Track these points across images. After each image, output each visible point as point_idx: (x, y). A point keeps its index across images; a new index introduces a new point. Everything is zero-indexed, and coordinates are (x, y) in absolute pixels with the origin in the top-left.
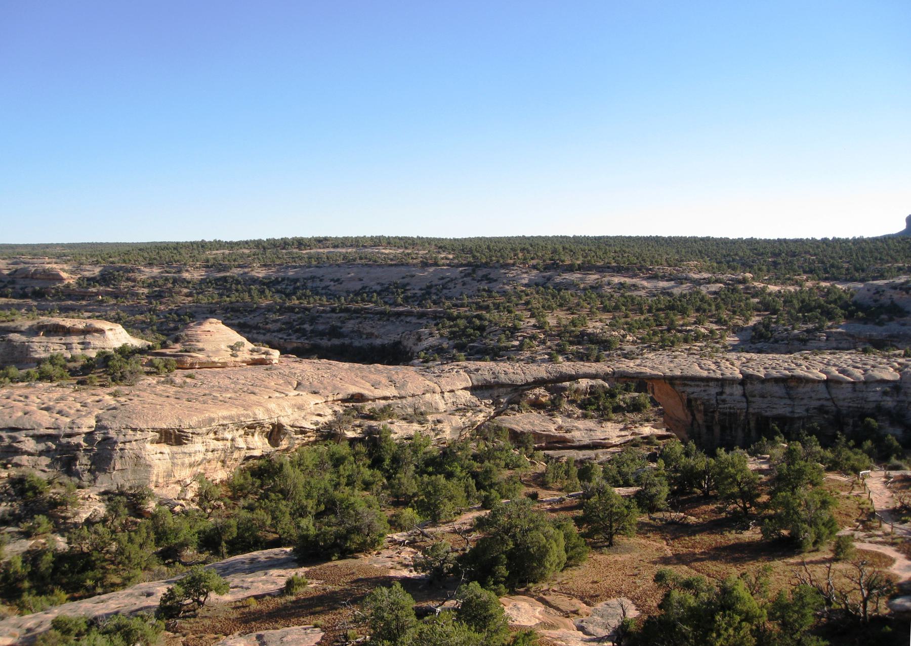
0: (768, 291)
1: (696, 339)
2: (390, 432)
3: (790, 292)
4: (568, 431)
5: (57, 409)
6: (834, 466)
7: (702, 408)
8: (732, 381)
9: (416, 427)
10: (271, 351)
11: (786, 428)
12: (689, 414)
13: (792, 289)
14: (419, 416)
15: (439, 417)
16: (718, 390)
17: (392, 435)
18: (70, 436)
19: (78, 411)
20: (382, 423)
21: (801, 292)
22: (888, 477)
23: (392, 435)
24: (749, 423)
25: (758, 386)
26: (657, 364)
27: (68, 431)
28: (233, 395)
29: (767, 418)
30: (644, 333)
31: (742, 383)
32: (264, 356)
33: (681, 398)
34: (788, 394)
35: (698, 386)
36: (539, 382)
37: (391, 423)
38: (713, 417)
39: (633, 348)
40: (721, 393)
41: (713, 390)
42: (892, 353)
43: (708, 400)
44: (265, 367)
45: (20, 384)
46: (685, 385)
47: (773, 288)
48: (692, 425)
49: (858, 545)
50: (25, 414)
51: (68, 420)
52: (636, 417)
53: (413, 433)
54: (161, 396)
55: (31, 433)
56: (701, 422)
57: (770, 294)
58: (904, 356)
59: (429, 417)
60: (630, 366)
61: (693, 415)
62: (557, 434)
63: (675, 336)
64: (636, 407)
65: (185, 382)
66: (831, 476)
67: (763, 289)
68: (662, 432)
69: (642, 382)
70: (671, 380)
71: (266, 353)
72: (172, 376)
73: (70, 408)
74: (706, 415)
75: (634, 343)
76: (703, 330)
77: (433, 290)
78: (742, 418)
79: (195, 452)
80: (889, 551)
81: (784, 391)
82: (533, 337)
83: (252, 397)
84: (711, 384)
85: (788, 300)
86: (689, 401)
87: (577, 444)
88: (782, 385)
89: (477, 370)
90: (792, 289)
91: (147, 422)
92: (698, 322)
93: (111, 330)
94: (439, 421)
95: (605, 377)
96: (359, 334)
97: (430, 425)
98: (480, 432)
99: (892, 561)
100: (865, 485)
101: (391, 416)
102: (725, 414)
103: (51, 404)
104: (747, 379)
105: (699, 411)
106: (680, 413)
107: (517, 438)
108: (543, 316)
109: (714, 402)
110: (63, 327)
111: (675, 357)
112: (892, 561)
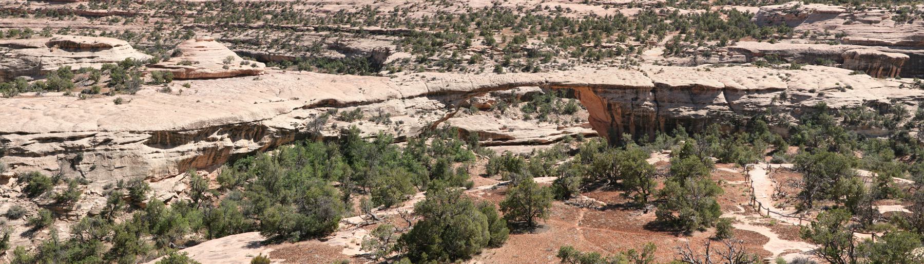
0: (680, 14)
1: (618, 53)
2: (359, 131)
3: (698, 14)
4: (511, 130)
5: (62, 115)
6: (725, 159)
7: (620, 111)
8: (645, 89)
9: (381, 127)
10: (258, 63)
11: (690, 128)
12: (609, 116)
13: (699, 12)
14: (382, 118)
15: (399, 119)
16: (634, 96)
17: (360, 135)
18: (73, 138)
19: (81, 116)
20: (353, 124)
21: (707, 15)
22: (770, 169)
23: (360, 135)
24: (659, 124)
25: (667, 93)
26: (583, 74)
27: (71, 134)
28: (223, 101)
29: (675, 119)
30: (573, 49)
31: (654, 90)
32: (252, 68)
33: (602, 103)
34: (692, 99)
35: (616, 93)
36: (483, 90)
37: (361, 124)
38: (629, 119)
39: (566, 61)
40: (636, 99)
41: (630, 97)
42: (781, 65)
43: (625, 105)
44: (253, 77)
45: (29, 94)
46: (606, 92)
47: (682, 12)
48: (612, 125)
49: (738, 226)
50: (31, 119)
51: (72, 125)
52: (568, 118)
53: (378, 133)
54: (158, 102)
55: (37, 136)
56: (619, 123)
57: (681, 17)
58: (791, 68)
59: (391, 119)
60: (557, 76)
61: (613, 117)
62: (500, 132)
63: (600, 51)
64: (570, 111)
65: (181, 91)
66: (722, 168)
67: (675, 14)
68: (589, 131)
69: (571, 91)
70: (594, 88)
71: (254, 66)
72: (169, 85)
73: (74, 114)
74: (623, 117)
75: (566, 57)
76: (623, 47)
77: (400, 13)
78: (654, 119)
79: (188, 151)
80: (765, 231)
81: (689, 97)
82: (483, 52)
83: (240, 103)
84: (627, 91)
85: (697, 19)
86: (609, 105)
87: (517, 141)
88: (687, 92)
89: (434, 79)
90: (699, 12)
91: (144, 125)
92: (621, 40)
93: (118, 46)
94: (401, 122)
95: (540, 84)
96: (568, 10)
97: (393, 125)
98: (430, 130)
99: (767, 240)
100: (748, 176)
101: (360, 118)
102: (639, 116)
103: (56, 110)
104: (658, 87)
105: (618, 114)
106: (602, 115)
107: (464, 134)
108: (490, 35)
109: (630, 106)
110: (74, 43)
111: (598, 69)
112: (767, 240)
